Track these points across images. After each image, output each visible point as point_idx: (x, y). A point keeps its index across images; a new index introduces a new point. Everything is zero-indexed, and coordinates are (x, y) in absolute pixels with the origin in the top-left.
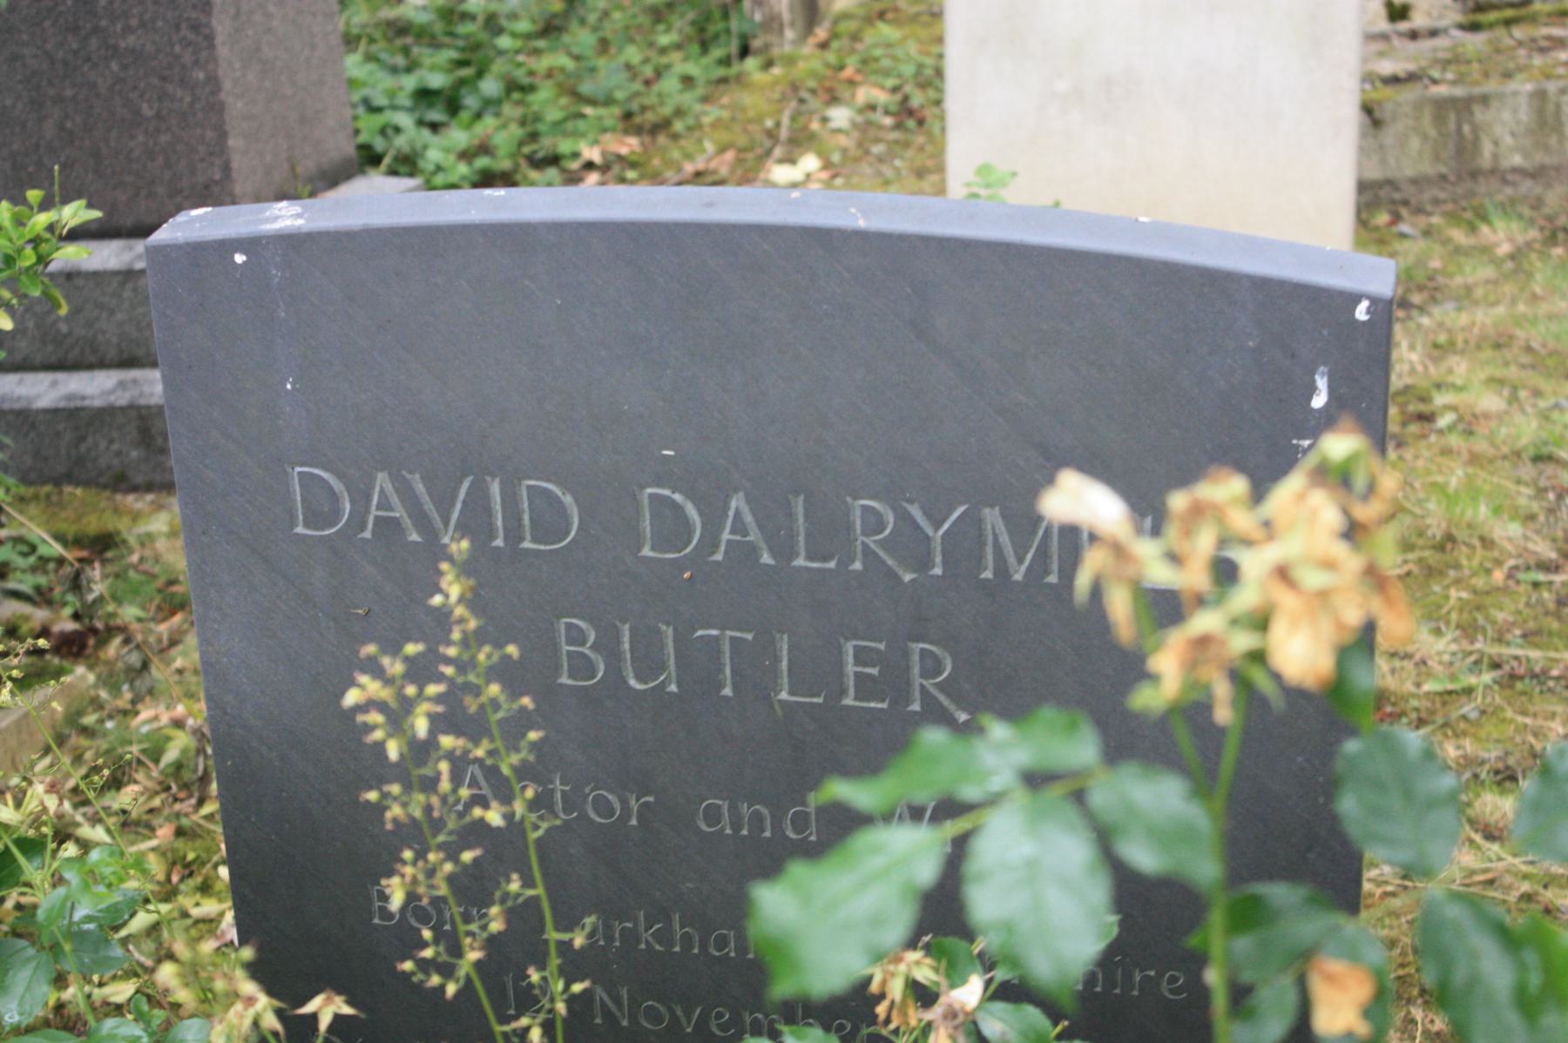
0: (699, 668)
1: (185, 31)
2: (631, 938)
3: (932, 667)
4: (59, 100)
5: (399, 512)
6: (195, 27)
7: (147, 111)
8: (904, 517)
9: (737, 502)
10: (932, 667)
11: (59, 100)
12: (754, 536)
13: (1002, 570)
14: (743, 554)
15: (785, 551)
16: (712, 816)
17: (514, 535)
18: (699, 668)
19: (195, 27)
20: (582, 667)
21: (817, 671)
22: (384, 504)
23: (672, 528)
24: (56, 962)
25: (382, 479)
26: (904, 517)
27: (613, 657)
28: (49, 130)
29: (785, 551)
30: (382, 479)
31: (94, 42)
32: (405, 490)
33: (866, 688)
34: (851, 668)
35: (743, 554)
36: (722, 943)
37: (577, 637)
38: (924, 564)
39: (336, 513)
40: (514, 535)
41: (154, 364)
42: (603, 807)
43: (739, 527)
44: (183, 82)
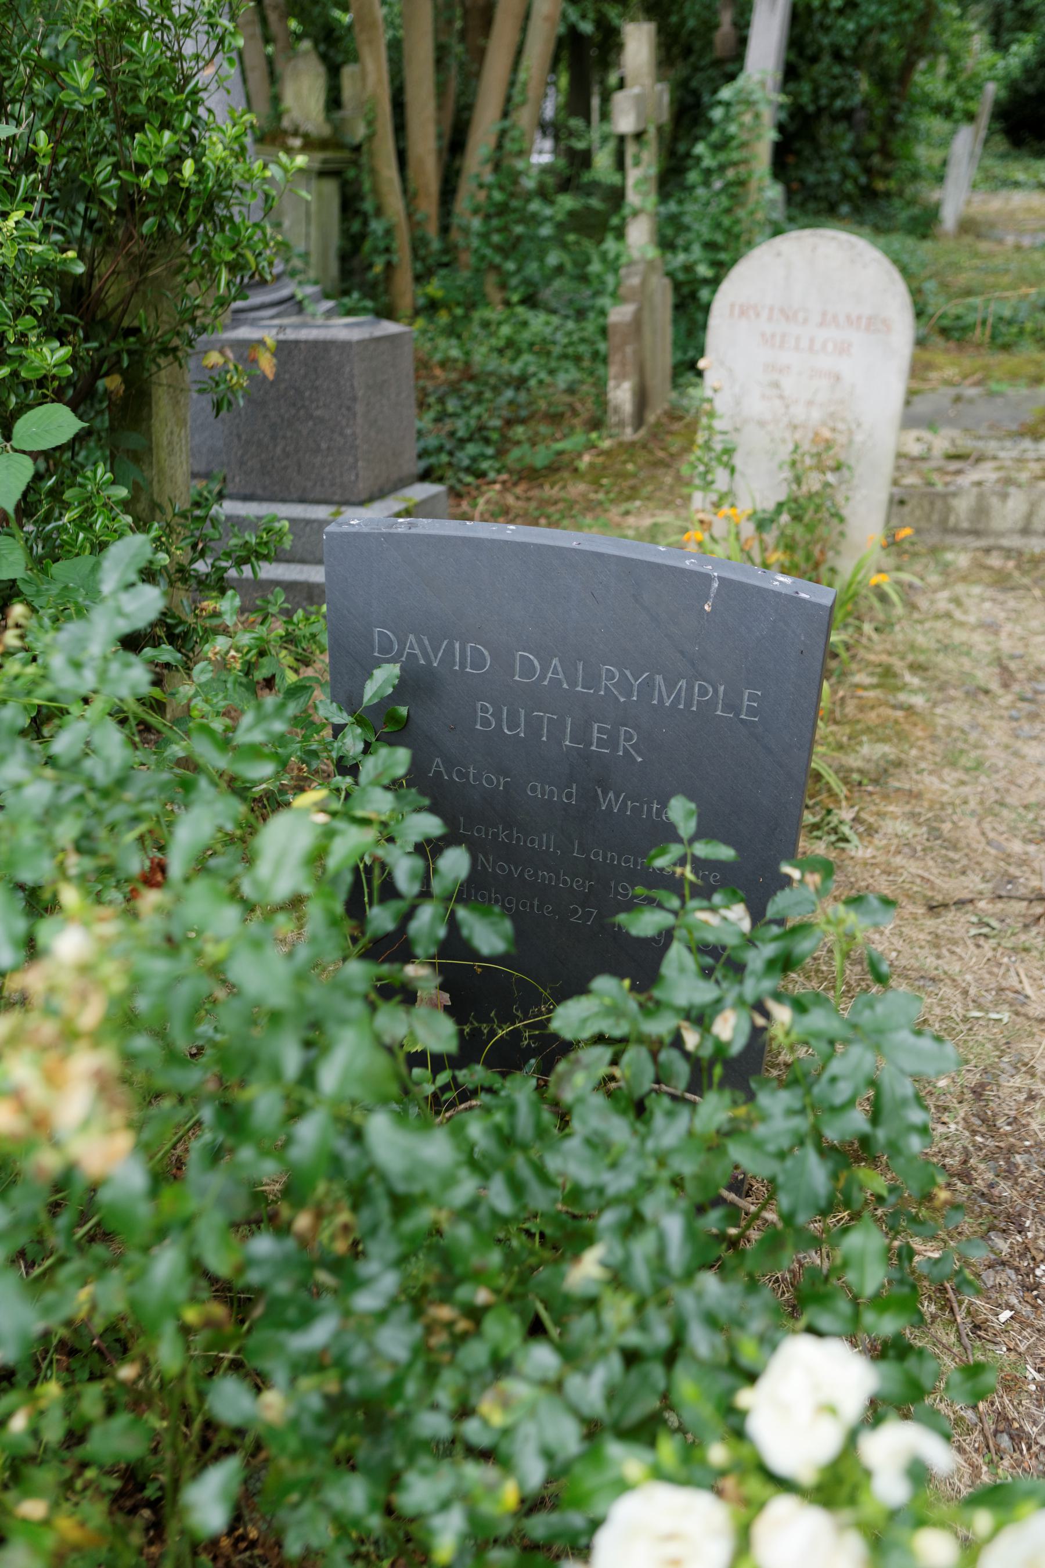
0: (534, 727)
1: (344, 411)
2: (495, 835)
3: (629, 738)
4: (284, 437)
5: (417, 652)
6: (349, 408)
7: (324, 446)
8: (623, 675)
9: (555, 661)
10: (629, 738)
11: (284, 437)
12: (561, 676)
13: (661, 700)
14: (556, 683)
15: (573, 684)
16: (534, 789)
17: (463, 665)
18: (534, 727)
19: (349, 408)
20: (486, 722)
21: (582, 734)
22: (411, 647)
23: (528, 669)
24: (64, 712)
25: (411, 637)
26: (623, 675)
27: (499, 721)
28: (279, 450)
29: (573, 684)
30: (411, 637)
31: (302, 412)
32: (420, 642)
33: (601, 743)
34: (595, 734)
35: (438, 773)
36: (532, 841)
37: (485, 710)
38: (629, 695)
39: (392, 649)
40: (463, 665)
41: (319, 562)
42: (489, 781)
43: (555, 672)
44: (341, 434)
